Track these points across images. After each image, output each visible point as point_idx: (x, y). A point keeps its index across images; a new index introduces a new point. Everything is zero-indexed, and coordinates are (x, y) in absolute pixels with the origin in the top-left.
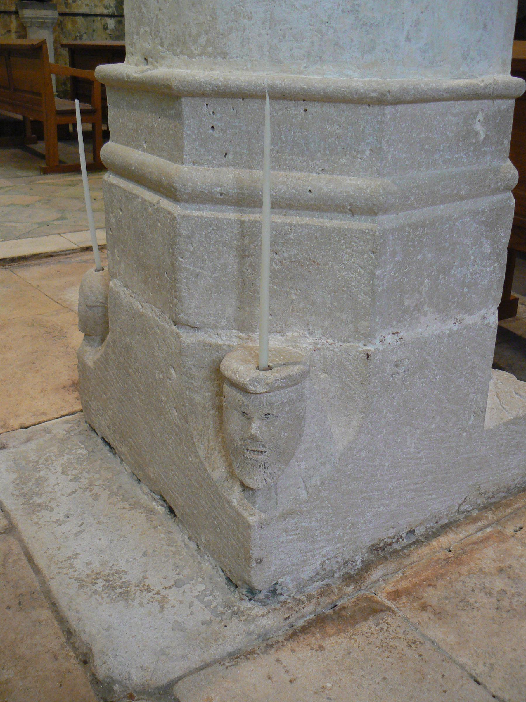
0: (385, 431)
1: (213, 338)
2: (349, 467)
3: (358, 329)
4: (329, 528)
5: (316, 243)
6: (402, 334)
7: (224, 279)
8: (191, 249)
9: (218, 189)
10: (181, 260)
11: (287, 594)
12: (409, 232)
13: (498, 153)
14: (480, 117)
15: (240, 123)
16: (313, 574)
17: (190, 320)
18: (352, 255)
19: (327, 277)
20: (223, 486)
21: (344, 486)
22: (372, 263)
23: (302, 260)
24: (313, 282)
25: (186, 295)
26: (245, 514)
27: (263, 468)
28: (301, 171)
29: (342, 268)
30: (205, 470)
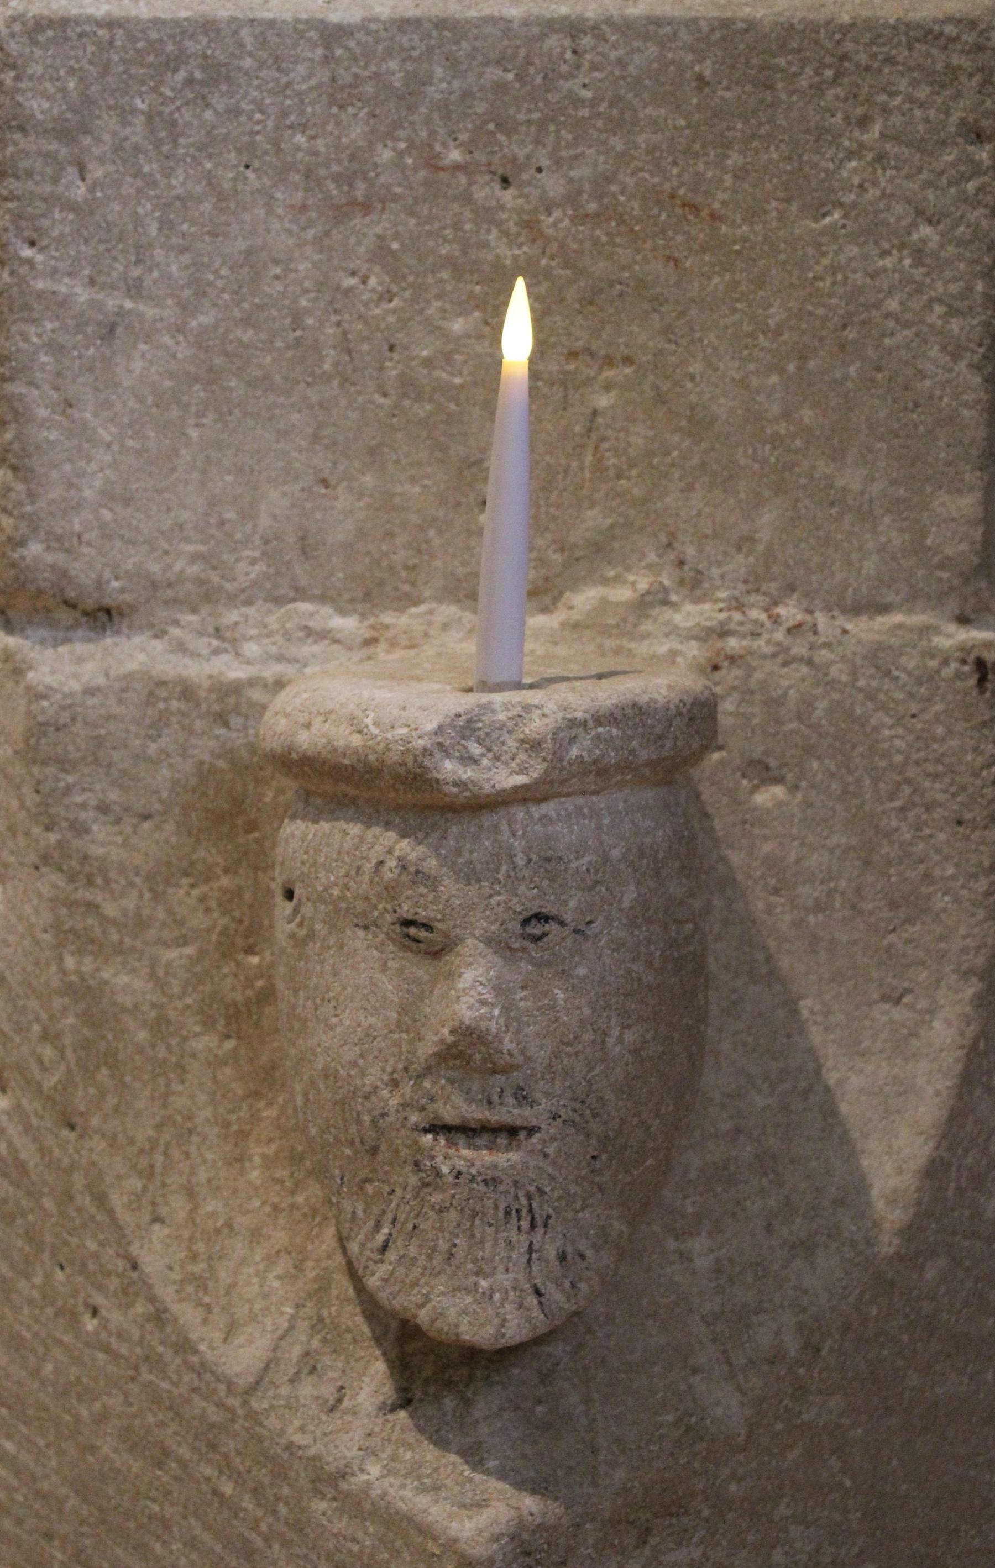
1: (195, 655)
2: (930, 1274)
3: (924, 533)
5: (698, 107)
7: (247, 335)
8: (80, 192)
10: (27, 252)
17: (76, 568)
18: (881, 158)
19: (760, 282)
20: (292, 1405)
21: (913, 1379)
22: (979, 190)
23: (636, 204)
24: (693, 312)
25: (53, 435)
26: (434, 1510)
27: (525, 1224)
30: (184, 1346)
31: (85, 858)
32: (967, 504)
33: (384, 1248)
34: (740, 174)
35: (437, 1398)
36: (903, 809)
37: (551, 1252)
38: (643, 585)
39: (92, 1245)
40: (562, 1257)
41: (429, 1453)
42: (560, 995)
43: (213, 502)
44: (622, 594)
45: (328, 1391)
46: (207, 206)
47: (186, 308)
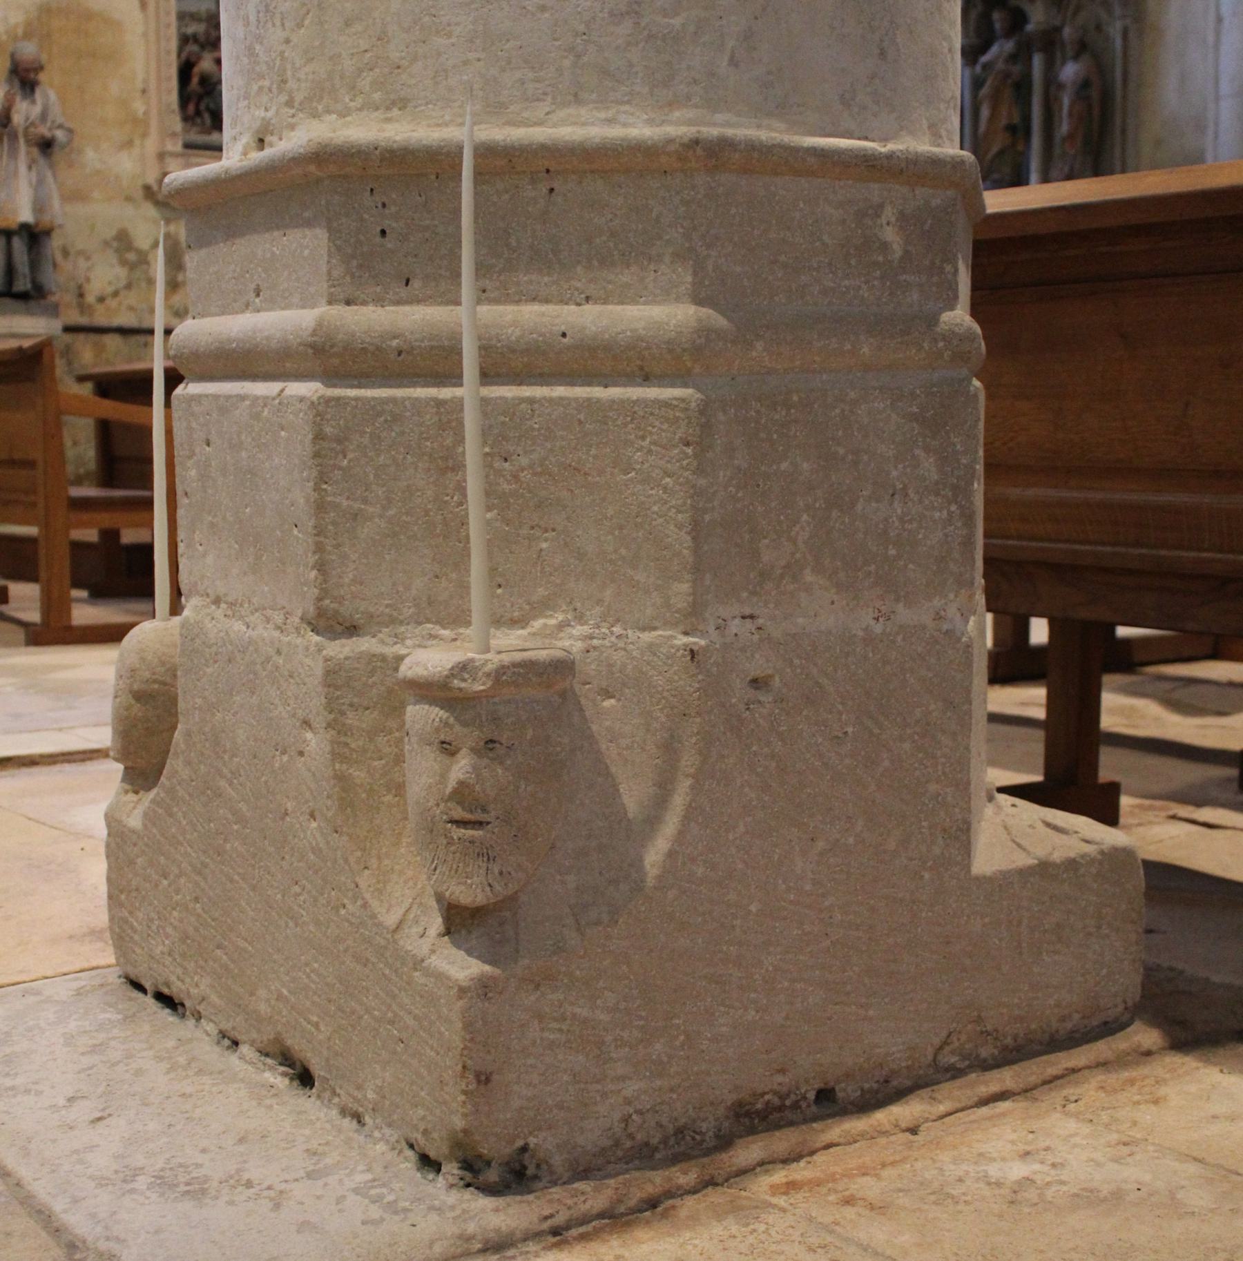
0: (741, 829)
1: (387, 644)
4: (636, 1033)
6: (761, 621)
7: (408, 519)
9: (395, 343)
11: (548, 1178)
12: (758, 412)
13: (934, 289)
14: (889, 213)
15: (433, 219)
16: (607, 1143)
17: (342, 610)
18: (650, 452)
25: (334, 557)
28: (547, 301)
29: (631, 480)
30: (373, 916)
31: (344, 725)
32: (685, 587)
33: (435, 869)
34: (595, 457)
35: (459, 931)
36: (661, 709)
37: (496, 871)
38: (560, 618)
39: (343, 879)
40: (501, 873)
41: (454, 951)
42: (500, 771)
43: (394, 584)
44: (553, 622)
45: (421, 930)
46: (393, 469)
47: (384, 508)
